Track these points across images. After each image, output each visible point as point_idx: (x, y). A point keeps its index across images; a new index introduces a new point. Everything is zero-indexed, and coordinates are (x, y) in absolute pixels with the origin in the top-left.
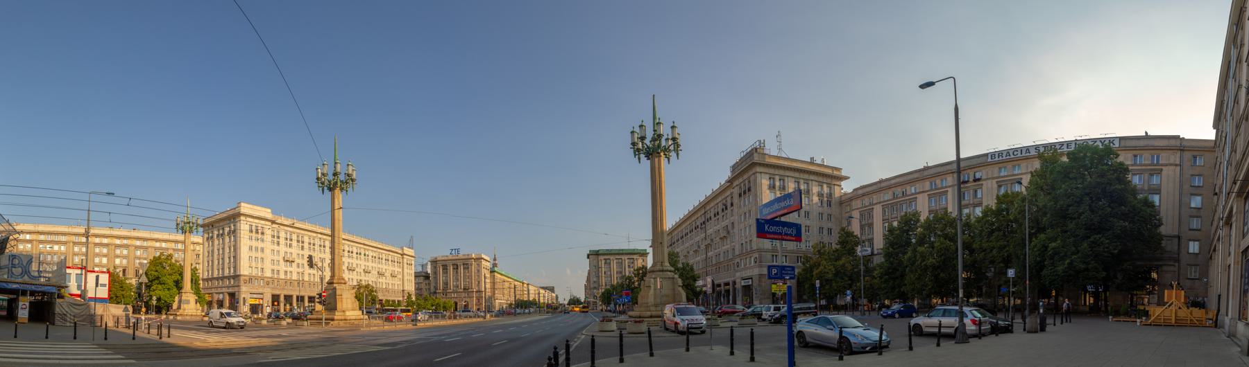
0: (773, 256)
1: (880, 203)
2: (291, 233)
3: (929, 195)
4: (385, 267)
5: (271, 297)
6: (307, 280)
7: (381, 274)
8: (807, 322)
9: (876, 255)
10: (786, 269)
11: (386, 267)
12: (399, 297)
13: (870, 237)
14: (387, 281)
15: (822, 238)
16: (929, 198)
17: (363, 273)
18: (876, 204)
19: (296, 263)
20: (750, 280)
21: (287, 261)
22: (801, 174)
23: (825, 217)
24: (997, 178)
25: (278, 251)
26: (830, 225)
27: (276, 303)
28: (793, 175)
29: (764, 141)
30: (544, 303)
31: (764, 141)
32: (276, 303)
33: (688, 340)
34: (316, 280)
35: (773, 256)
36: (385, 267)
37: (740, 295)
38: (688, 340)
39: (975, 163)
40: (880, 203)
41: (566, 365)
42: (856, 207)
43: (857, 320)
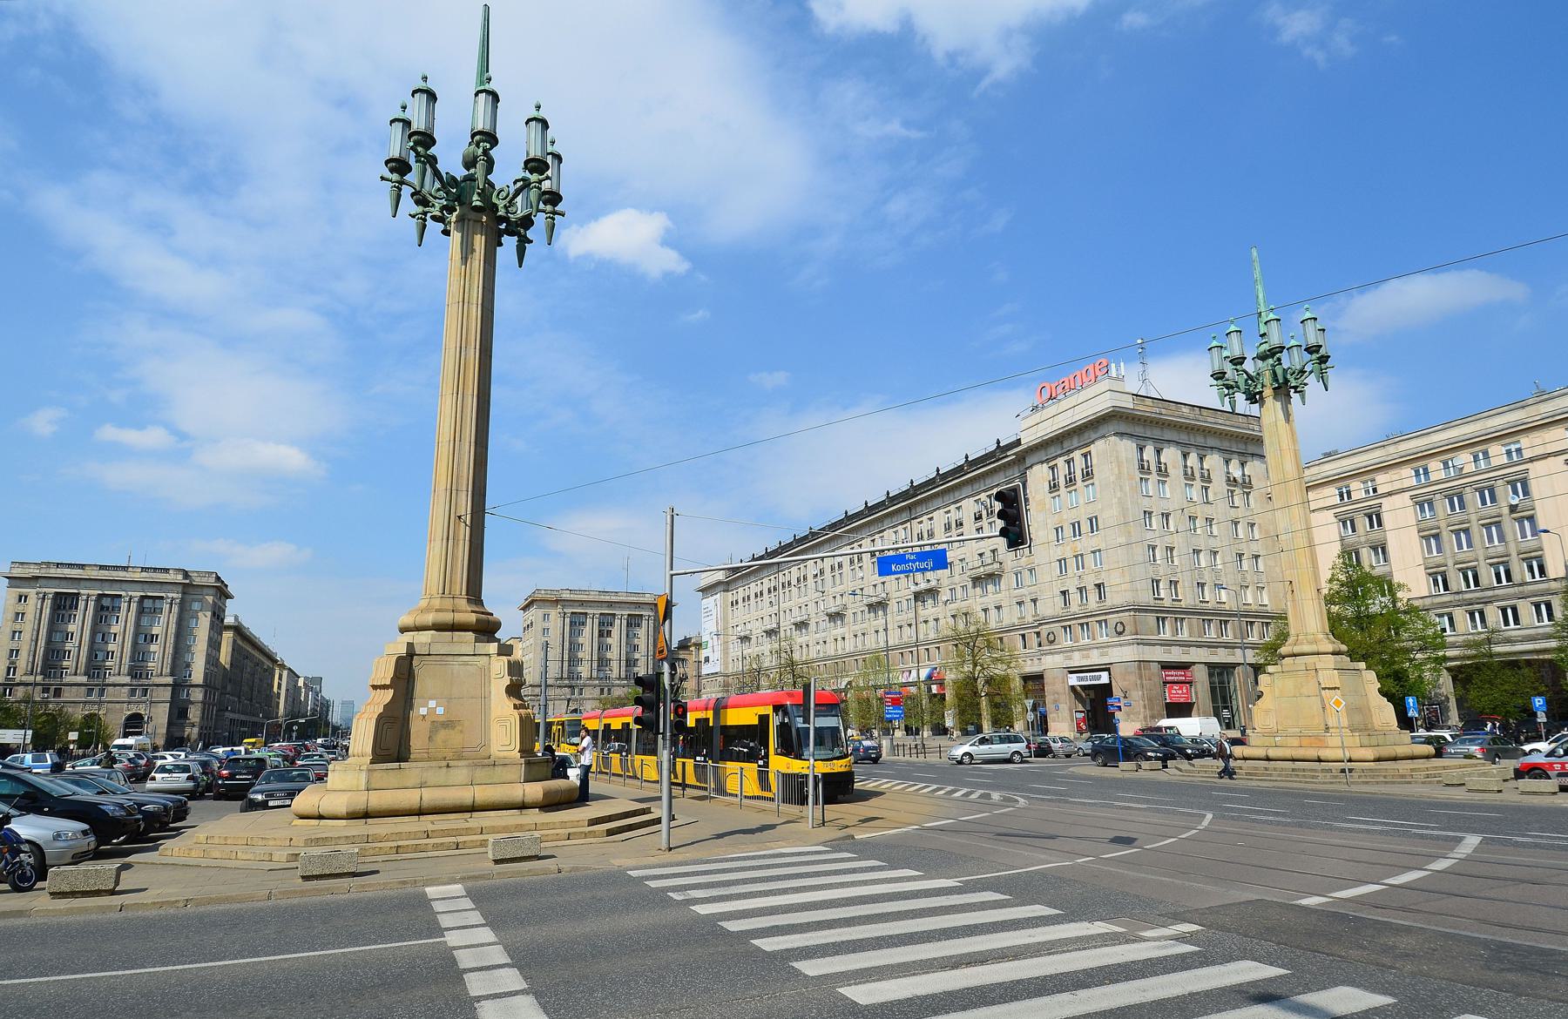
0: (1158, 618)
1: (1403, 491)
3: (1412, 497)
20: (1105, 675)
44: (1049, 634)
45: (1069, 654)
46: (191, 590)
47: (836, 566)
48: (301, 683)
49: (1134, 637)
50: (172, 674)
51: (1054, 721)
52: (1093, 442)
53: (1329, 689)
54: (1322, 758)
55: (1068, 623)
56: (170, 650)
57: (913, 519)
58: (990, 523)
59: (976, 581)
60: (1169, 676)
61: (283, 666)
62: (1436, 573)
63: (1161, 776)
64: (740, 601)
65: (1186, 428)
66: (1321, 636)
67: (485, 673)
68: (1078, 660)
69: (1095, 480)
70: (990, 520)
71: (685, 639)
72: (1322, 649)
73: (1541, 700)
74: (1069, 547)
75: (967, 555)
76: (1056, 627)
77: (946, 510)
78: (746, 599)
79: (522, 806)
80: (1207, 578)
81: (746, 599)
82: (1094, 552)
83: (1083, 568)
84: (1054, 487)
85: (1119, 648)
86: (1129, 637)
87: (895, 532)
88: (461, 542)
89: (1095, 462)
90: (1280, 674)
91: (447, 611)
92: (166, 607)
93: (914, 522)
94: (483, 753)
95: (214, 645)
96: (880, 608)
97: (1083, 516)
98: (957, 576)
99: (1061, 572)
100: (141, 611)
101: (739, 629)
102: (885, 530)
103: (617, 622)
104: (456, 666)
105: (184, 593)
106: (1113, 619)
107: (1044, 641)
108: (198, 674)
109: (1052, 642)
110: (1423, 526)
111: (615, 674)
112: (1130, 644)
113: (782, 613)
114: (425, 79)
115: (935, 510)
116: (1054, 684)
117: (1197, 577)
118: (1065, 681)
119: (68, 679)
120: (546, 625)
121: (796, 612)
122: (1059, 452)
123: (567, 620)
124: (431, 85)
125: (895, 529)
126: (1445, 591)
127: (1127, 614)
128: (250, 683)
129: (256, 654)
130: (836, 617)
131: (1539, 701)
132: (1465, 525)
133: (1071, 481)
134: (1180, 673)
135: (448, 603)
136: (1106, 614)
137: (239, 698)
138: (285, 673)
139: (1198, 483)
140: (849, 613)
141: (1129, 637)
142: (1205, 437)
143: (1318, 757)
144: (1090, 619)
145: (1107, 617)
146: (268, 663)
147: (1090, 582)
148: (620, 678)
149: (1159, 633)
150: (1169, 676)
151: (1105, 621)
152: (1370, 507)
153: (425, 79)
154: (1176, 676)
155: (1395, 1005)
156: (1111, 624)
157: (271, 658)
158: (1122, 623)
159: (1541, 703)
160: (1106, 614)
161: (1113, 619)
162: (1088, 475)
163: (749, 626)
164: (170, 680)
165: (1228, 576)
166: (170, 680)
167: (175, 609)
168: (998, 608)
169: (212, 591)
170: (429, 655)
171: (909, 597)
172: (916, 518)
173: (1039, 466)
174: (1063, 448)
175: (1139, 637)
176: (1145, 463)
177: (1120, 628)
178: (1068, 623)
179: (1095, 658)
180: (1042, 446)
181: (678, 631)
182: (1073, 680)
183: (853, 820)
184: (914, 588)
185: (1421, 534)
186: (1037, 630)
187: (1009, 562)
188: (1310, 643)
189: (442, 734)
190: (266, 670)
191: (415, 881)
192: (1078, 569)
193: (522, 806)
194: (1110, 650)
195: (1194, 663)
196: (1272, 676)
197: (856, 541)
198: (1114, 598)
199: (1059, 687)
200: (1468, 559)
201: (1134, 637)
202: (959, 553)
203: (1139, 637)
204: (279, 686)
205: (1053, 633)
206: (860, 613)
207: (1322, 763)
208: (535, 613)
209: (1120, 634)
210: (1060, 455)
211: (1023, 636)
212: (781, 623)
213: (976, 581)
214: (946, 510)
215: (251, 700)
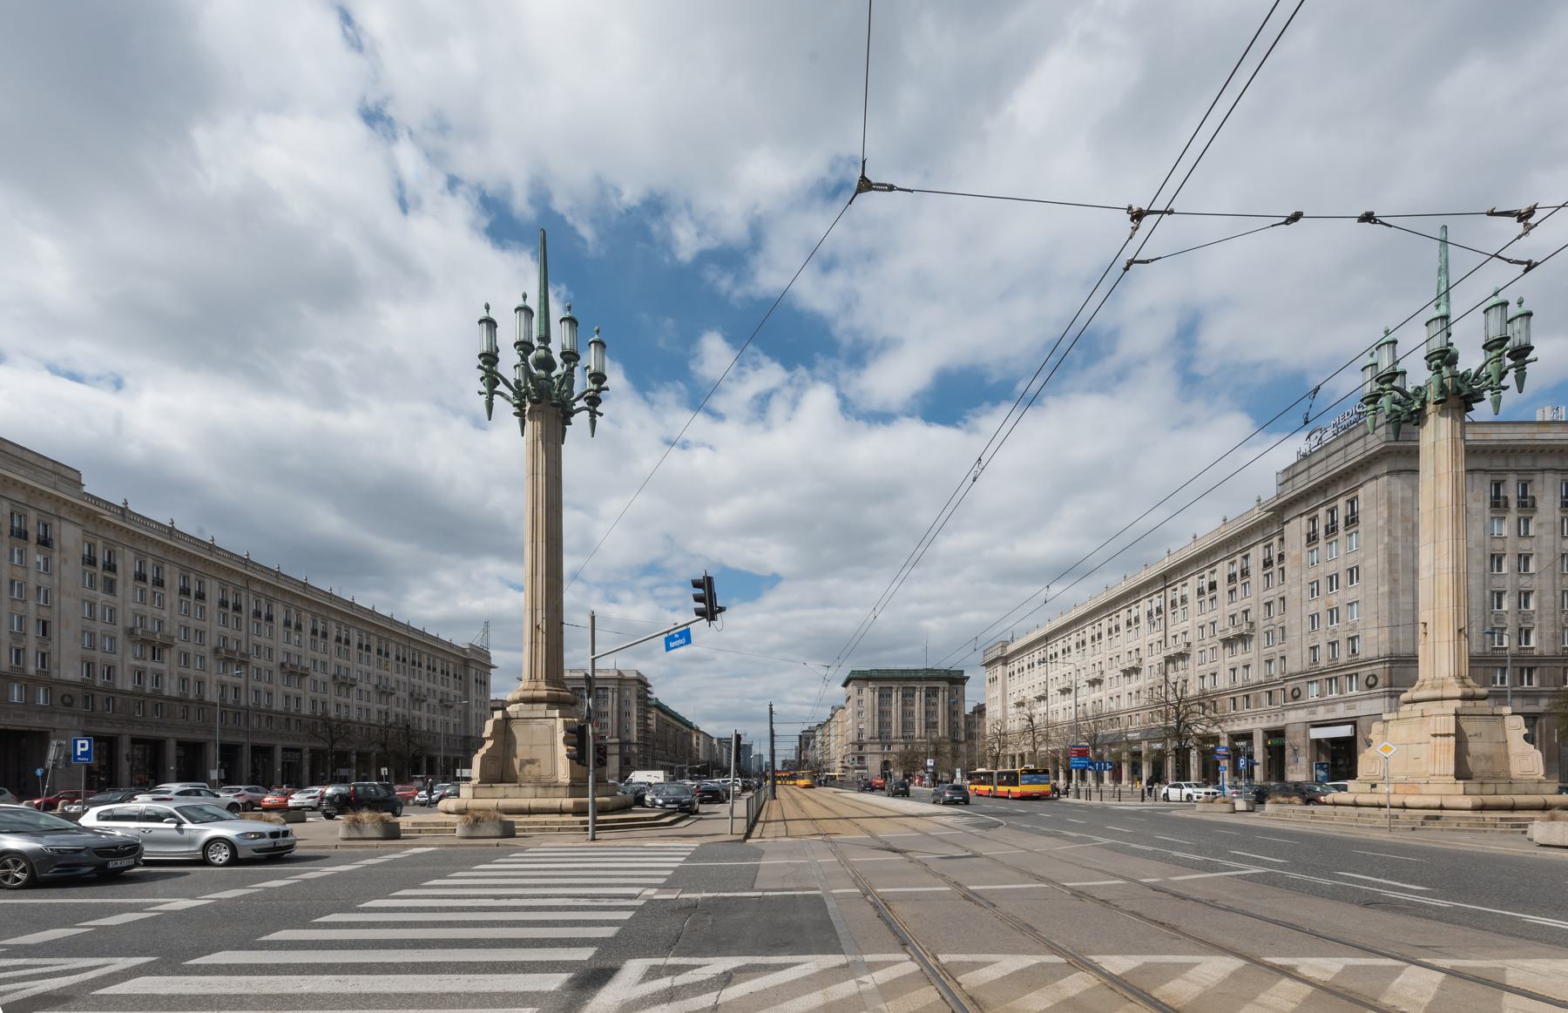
2: (348, 628)
4: (428, 685)
6: (129, 687)
7: (417, 699)
10: (908, 948)
11: (431, 685)
14: (364, 703)
17: (373, 695)
19: (175, 651)
20: (1349, 727)
21: (292, 673)
25: (324, 664)
30: (313, 716)
33: (1448, 735)
34: (243, 703)
36: (428, 685)
38: (1448, 735)
39: (1485, 429)
41: (3, 967)
43: (138, 956)
44: (1294, 690)
45: (1313, 709)
46: (623, 683)
47: (1096, 636)
48: (715, 742)
49: (1387, 689)
50: (618, 737)
51: (1292, 772)
52: (1361, 485)
53: (1441, 735)
54: (1407, 805)
55: (1334, 675)
56: (615, 721)
57: (1168, 587)
58: (1245, 584)
59: (1228, 642)
61: (698, 730)
63: (1253, 820)
64: (1016, 672)
65: (1532, 451)
66: (1452, 680)
67: (553, 729)
68: (1322, 714)
69: (1361, 528)
70: (1244, 581)
71: (979, 705)
72: (1447, 693)
74: (1323, 601)
76: (1301, 683)
77: (1201, 574)
78: (1021, 670)
79: (561, 812)
81: (1021, 670)
82: (1351, 604)
83: (1337, 622)
84: (1312, 538)
85: (1369, 702)
86: (1382, 690)
87: (1151, 601)
88: (540, 645)
89: (1361, 506)
90: (1396, 721)
91: (530, 690)
92: (610, 694)
93: (1169, 590)
94: (553, 779)
95: (643, 719)
97: (1340, 567)
98: (1208, 639)
99: (1313, 628)
100: (927, 695)
101: (1015, 696)
102: (1140, 600)
103: (917, 693)
104: (534, 726)
105: (620, 685)
106: (1365, 672)
107: (1289, 697)
108: (634, 735)
109: (1296, 698)
111: (893, 735)
112: (1377, 697)
113: (1049, 681)
114: (487, 307)
115: (1189, 576)
116: (1295, 737)
117: (1493, 622)
118: (1306, 734)
119: (609, 741)
120: (860, 698)
121: (1061, 679)
123: (877, 693)
124: (492, 315)
125: (1150, 599)
127: (1381, 666)
128: (674, 742)
129: (676, 723)
130: (1096, 682)
133: (1331, 530)
135: (533, 685)
136: (1357, 667)
137: (666, 751)
138: (701, 736)
139: (1512, 516)
140: (1106, 678)
141: (1382, 690)
143: (1403, 803)
144: (1339, 674)
145: (1359, 670)
146: (686, 729)
147: (1342, 637)
148: (920, 738)
149: (1522, 683)
151: (1357, 674)
153: (487, 307)
155: (620, 931)
156: (1363, 677)
157: (689, 725)
158: (1374, 676)
160: (1357, 667)
161: (1365, 672)
162: (1352, 520)
163: (1023, 694)
164: (617, 740)
165: (1545, 618)
166: (617, 740)
167: (615, 695)
168: (1247, 667)
169: (636, 683)
170: (518, 718)
171: (1161, 661)
172: (1170, 586)
173: (1299, 519)
174: (1326, 497)
175: (1393, 689)
176: (1502, 500)
177: (1371, 681)
178: (1334, 675)
179: (1341, 711)
180: (1302, 497)
181: (971, 698)
182: (1317, 734)
183: (174, 791)
184: (1165, 653)
186: (1283, 687)
187: (1261, 622)
188: (1433, 687)
189: (528, 767)
190: (685, 734)
192: (1332, 623)
193: (561, 812)
194: (1358, 703)
196: (1386, 724)
197: (1115, 612)
198: (1366, 650)
199: (1299, 741)
201: (1387, 689)
202: (1211, 616)
203: (1393, 689)
204: (698, 744)
205: (1298, 689)
206: (1115, 678)
207: (1407, 810)
208: (852, 688)
209: (1371, 687)
210: (1322, 505)
211: (1270, 693)
212: (1049, 690)
213: (1228, 642)
214: (1201, 574)
215: (676, 753)
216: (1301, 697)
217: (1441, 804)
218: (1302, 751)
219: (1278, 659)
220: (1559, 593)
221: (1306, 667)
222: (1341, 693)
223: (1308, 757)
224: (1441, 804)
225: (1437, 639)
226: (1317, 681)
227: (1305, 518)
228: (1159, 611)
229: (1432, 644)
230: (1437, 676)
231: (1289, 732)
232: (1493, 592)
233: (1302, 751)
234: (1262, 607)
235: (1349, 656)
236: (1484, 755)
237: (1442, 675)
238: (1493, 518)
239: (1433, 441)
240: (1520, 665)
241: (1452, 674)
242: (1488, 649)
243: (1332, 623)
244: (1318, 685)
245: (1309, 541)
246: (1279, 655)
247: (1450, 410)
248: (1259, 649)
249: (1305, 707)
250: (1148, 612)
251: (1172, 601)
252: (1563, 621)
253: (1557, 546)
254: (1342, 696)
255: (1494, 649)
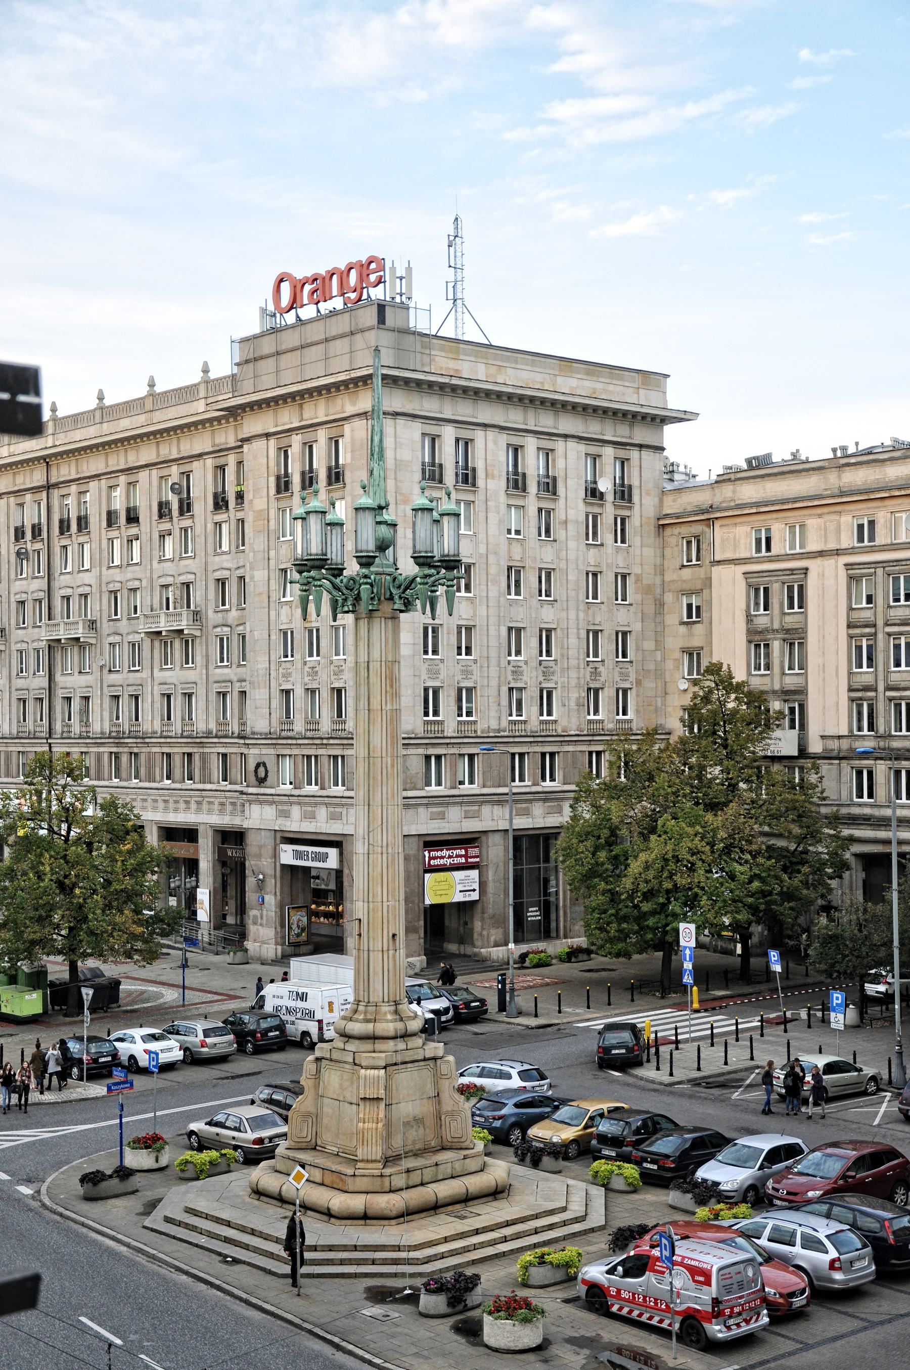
0: (428, 758)
1: (838, 552)
3: (849, 566)
5: (28, 1273)
8: (567, 1301)
9: (816, 757)
12: (20, 896)
13: (791, 682)
15: (595, 673)
16: (851, 578)
18: (821, 554)
20: (333, 852)
22: (531, 414)
23: (606, 584)
24: (851, 551)
26: (623, 618)
27: (533, 914)
28: (409, 408)
29: (409, 269)
31: (409, 269)
32: (533, 914)
35: (428, 758)
37: (271, 900)
40: (838, 552)
42: (729, 555)
44: (258, 766)
51: (255, 923)
60: (435, 858)
62: (861, 699)
68: (296, 823)
73: (839, 996)
75: (145, 583)
80: (531, 679)
93: (56, 493)
96: (76, 649)
109: (261, 781)
110: (855, 615)
116: (259, 856)
117: (510, 678)
118: (275, 855)
122: (296, 424)
126: (869, 731)
131: (837, 999)
132: (867, 630)
134: (458, 852)
142: (631, 425)
147: (325, 682)
150: (435, 858)
152: (792, 571)
154: (450, 857)
159: (839, 1002)
182: (288, 855)
185: (851, 631)
191: (448, 645)
195: (485, 832)
200: (903, 684)
202: (129, 576)
205: (264, 764)
216: (268, 783)
217: (365, 1213)
218: (271, 883)
219: (236, 694)
220: (583, 634)
221: (276, 727)
222: (322, 788)
223: (279, 897)
224: (365, 1213)
225: (371, 949)
226: (290, 756)
227: (272, 442)
228: (36, 530)
229: (366, 953)
230: (371, 1000)
231: (253, 842)
232: (510, 629)
233: (271, 883)
234: (212, 586)
235: (333, 722)
236: (415, 1119)
237: (376, 1000)
238: (509, 506)
239: (366, 660)
240: (539, 749)
241: (386, 999)
242: (504, 724)
243: (311, 655)
244: (292, 760)
245: (278, 491)
246: (237, 687)
247: (383, 619)
248: (207, 669)
249: (274, 802)
250: (16, 529)
251: (61, 521)
252: (588, 679)
253: (581, 558)
254: (324, 793)
255: (511, 722)
